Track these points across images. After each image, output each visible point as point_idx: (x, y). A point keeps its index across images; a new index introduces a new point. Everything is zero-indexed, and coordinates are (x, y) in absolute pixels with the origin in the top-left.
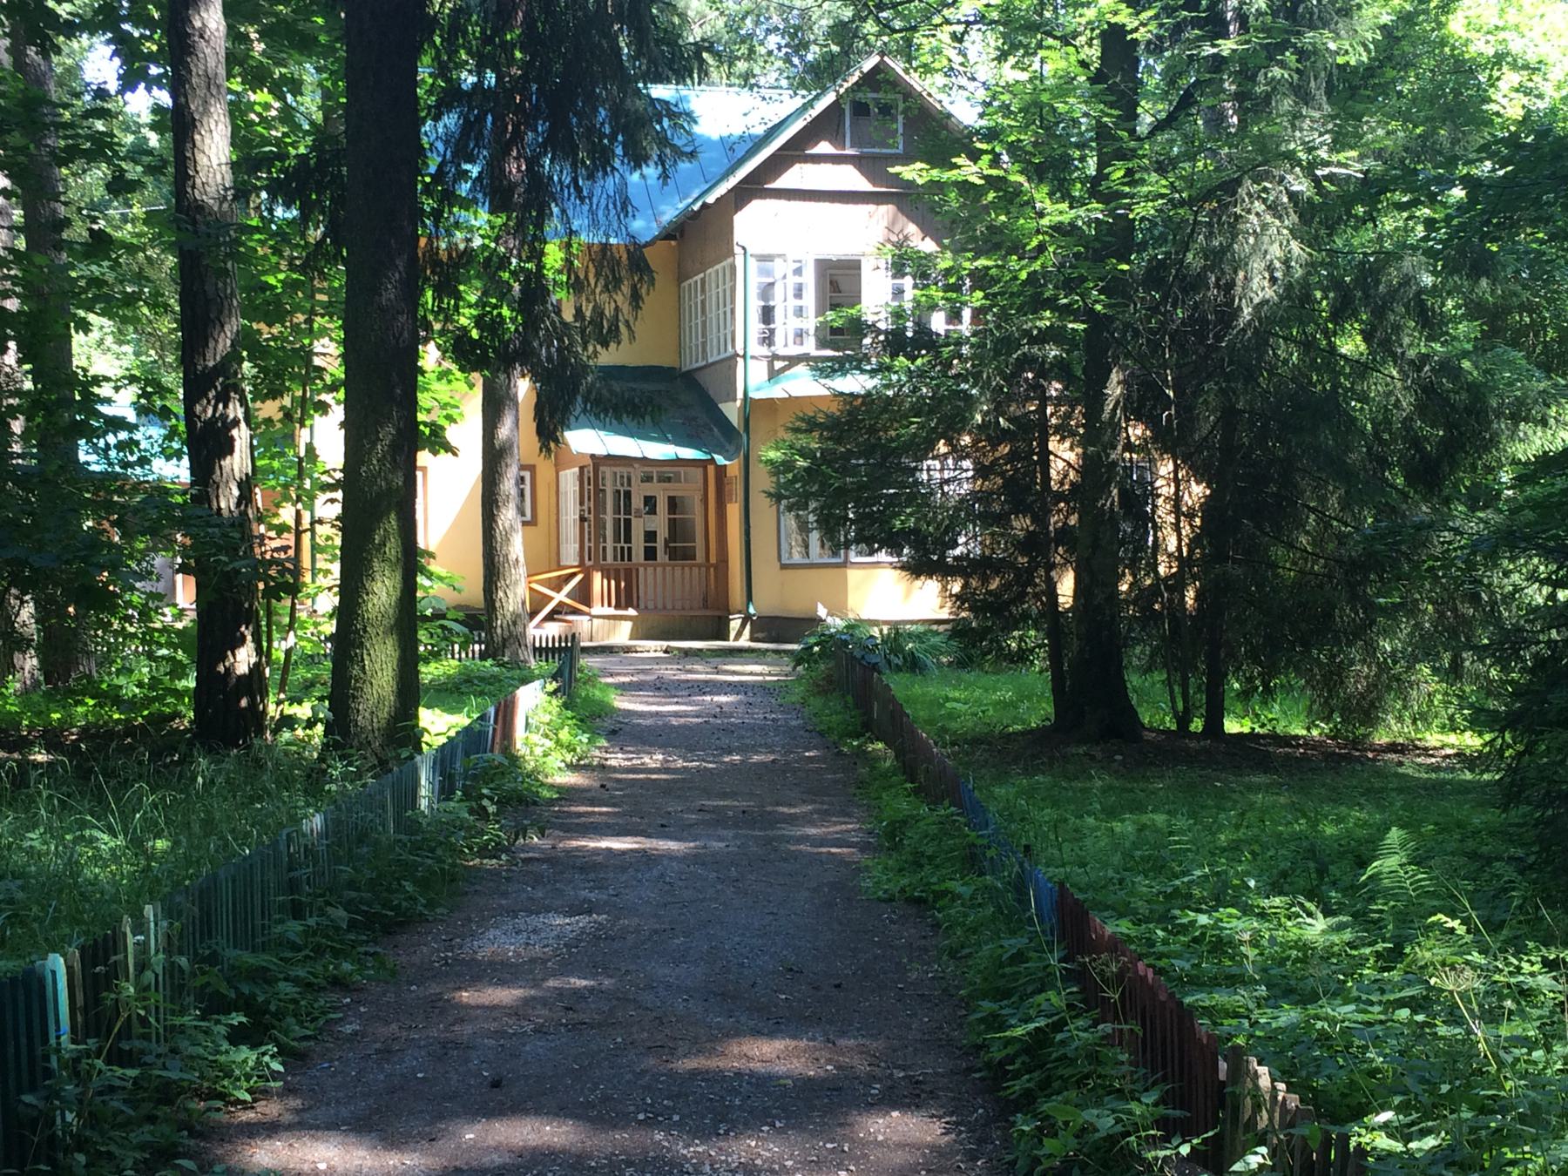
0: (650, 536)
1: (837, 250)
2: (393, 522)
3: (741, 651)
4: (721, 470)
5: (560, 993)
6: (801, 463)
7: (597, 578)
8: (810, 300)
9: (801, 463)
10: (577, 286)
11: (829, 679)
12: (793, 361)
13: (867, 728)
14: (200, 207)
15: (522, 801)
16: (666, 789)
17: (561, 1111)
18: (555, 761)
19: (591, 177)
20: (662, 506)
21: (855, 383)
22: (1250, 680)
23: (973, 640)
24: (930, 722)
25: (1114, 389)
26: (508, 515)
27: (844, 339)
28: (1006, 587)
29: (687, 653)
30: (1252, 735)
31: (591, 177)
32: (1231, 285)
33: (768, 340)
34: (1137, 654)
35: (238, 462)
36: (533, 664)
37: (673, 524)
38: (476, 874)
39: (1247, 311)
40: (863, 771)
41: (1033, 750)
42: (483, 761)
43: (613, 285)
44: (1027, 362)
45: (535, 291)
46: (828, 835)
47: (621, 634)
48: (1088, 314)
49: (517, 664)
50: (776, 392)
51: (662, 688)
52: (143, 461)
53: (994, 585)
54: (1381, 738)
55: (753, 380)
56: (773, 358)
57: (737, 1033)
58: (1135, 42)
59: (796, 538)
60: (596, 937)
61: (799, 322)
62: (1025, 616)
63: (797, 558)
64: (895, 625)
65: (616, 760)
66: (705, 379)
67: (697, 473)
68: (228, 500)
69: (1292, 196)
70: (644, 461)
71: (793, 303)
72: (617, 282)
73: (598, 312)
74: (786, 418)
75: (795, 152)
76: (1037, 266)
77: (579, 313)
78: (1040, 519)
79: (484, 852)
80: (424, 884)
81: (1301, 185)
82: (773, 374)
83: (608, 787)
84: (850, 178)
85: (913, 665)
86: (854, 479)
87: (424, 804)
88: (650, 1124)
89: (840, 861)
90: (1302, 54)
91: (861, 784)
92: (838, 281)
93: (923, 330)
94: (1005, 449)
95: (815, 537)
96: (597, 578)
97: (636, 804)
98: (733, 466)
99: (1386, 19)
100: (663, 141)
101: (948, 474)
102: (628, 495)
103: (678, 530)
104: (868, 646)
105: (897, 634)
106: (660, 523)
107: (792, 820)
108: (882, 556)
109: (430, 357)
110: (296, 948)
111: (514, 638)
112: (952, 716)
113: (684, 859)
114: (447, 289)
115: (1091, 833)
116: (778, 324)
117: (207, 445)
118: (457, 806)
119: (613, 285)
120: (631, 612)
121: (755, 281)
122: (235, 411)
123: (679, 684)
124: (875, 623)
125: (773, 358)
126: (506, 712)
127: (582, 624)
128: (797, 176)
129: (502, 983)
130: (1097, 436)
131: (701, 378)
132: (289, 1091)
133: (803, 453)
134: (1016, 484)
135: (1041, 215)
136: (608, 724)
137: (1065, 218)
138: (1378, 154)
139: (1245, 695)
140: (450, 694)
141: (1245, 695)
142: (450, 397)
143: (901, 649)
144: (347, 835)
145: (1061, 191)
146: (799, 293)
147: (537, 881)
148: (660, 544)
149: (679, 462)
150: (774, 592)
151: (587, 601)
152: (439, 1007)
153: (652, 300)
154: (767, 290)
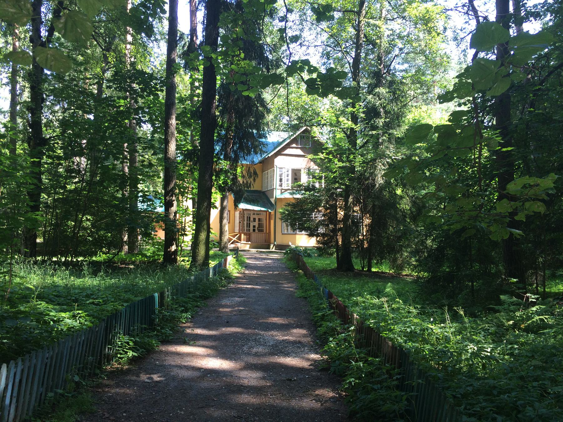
0: (254, 226)
1: (296, 167)
2: (205, 222)
3: (273, 252)
4: (270, 213)
5: (238, 310)
6: (287, 213)
7: (243, 235)
8: (290, 182)
9: (287, 213)
10: (243, 177)
11: (291, 258)
12: (286, 190)
13: (299, 267)
14: (169, 158)
15: (229, 278)
16: (257, 277)
17: (239, 327)
18: (235, 271)
19: (247, 155)
20: (257, 220)
21: (298, 196)
22: (378, 260)
23: (321, 251)
24: (312, 267)
25: (351, 200)
26: (225, 221)
27: (297, 187)
28: (328, 239)
29: (261, 252)
30: (378, 272)
31: (247, 155)
32: (374, 180)
33: (281, 185)
34: (354, 255)
35: (174, 209)
36: (229, 252)
37: (259, 224)
38: (221, 290)
39: (377, 185)
40: (297, 276)
41: (332, 273)
42: (221, 269)
43: (250, 177)
44: (333, 193)
45: (235, 179)
46: (288, 286)
47: (247, 247)
48: (345, 185)
49: (225, 252)
50: (282, 197)
51: (256, 258)
52: (155, 208)
53: (326, 239)
54: (404, 273)
55: (277, 194)
56: (282, 189)
57: (270, 317)
58: (356, 131)
59: (285, 228)
60: (244, 301)
61: (288, 183)
62: (332, 246)
63: (286, 232)
64: (306, 247)
65: (247, 272)
66: (267, 193)
67: (265, 213)
68: (172, 217)
69: (387, 162)
70: (253, 210)
71: (286, 183)
72: (251, 176)
73: (247, 182)
74: (284, 203)
75: (288, 146)
76: (335, 175)
77: (243, 182)
78: (335, 226)
79: (222, 286)
80: (212, 290)
81: (389, 160)
82: (282, 193)
83: (245, 276)
84: (299, 152)
85: (309, 256)
86: (298, 216)
87: (211, 276)
88: (255, 329)
89: (291, 291)
90: (389, 134)
91: (297, 278)
92: (296, 175)
93: (314, 186)
94: (328, 211)
95: (289, 227)
96: (243, 235)
97: (251, 280)
98: (272, 212)
99: (407, 128)
100: (261, 150)
101: (318, 216)
102: (250, 217)
103: (260, 225)
104: (300, 251)
105: (306, 249)
106: (256, 224)
107: (282, 284)
108: (303, 232)
109: (213, 190)
110: (191, 298)
111: (225, 247)
112: (317, 266)
113: (261, 289)
114: (218, 176)
115: (339, 287)
116: (283, 182)
117: (168, 205)
118: (217, 277)
119: (250, 177)
120: (250, 243)
121: (278, 173)
122: (174, 198)
123: (260, 258)
124: (301, 247)
125: (282, 189)
126: (226, 260)
127: (239, 245)
128: (288, 151)
129: (227, 308)
130: (347, 208)
131: (266, 193)
132: (191, 322)
133: (287, 210)
134: (332, 218)
135: (336, 164)
136: (245, 265)
137: (341, 165)
138: (405, 154)
139: (377, 264)
140: (215, 257)
141: (377, 264)
142: (216, 197)
143: (307, 252)
144: (199, 279)
145: (340, 160)
146: (288, 181)
147: (233, 292)
148: (256, 229)
149: (261, 211)
150: (280, 239)
151: (240, 240)
152: (215, 311)
153: (258, 180)
154: (281, 175)
